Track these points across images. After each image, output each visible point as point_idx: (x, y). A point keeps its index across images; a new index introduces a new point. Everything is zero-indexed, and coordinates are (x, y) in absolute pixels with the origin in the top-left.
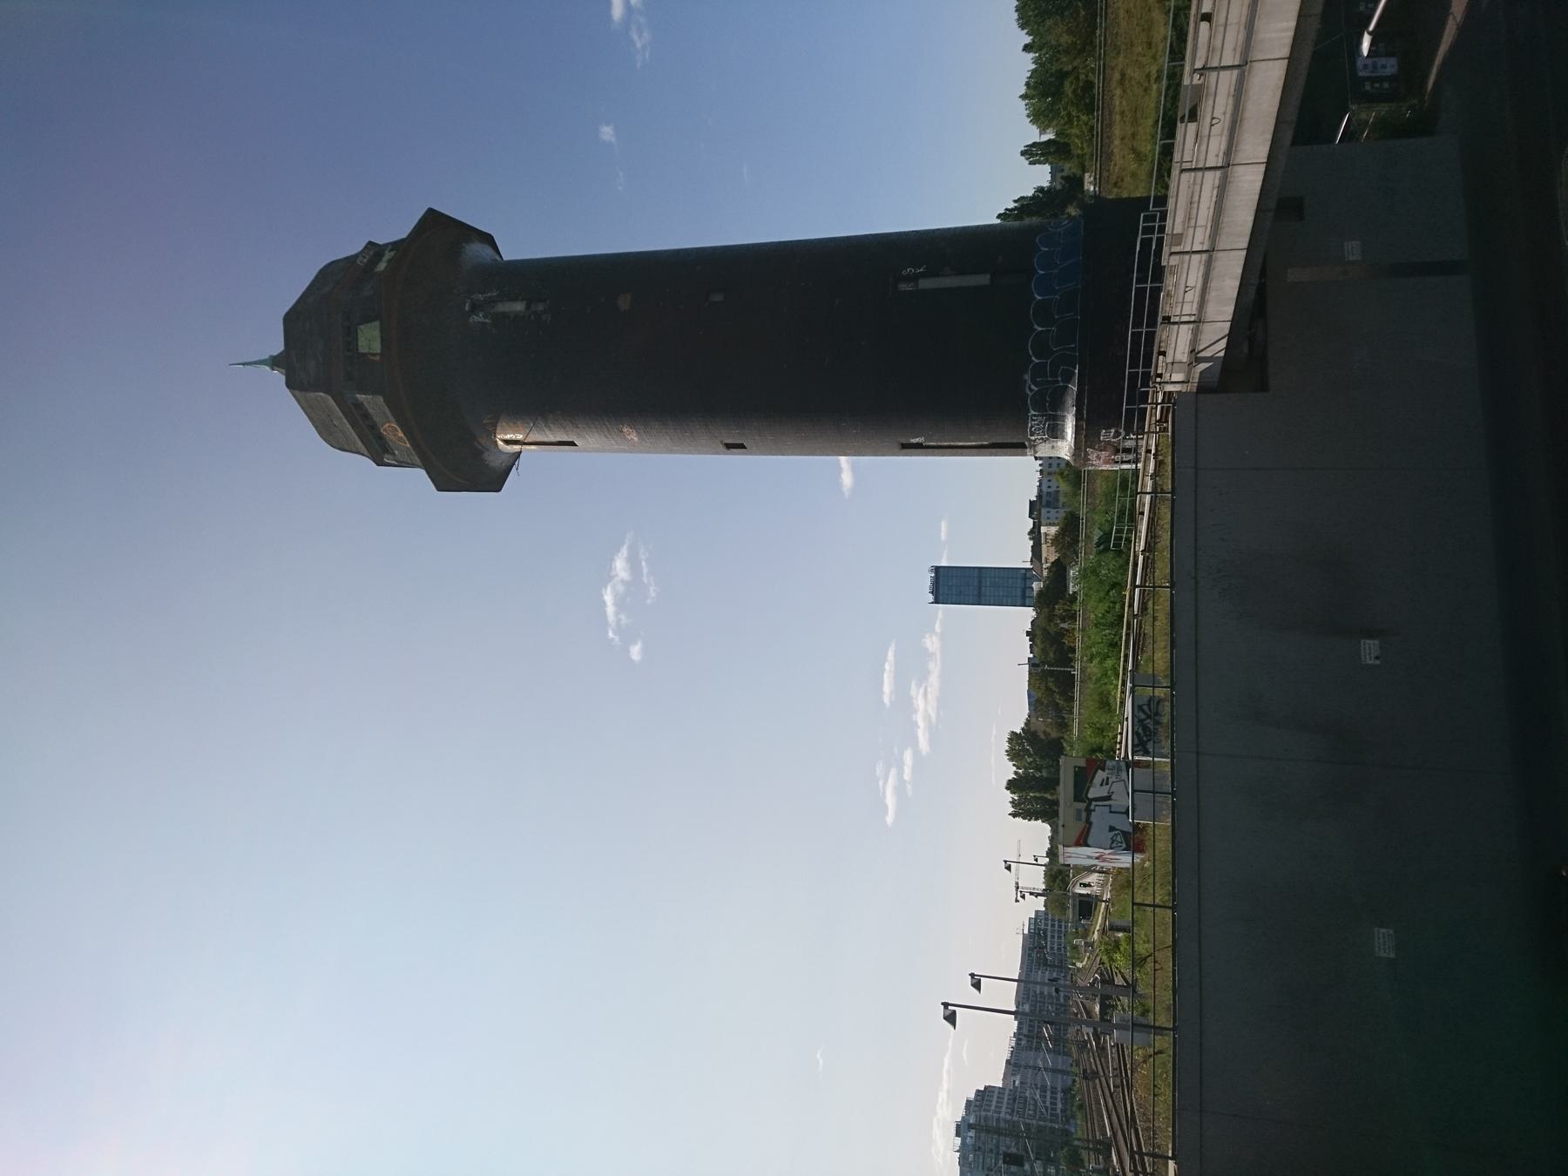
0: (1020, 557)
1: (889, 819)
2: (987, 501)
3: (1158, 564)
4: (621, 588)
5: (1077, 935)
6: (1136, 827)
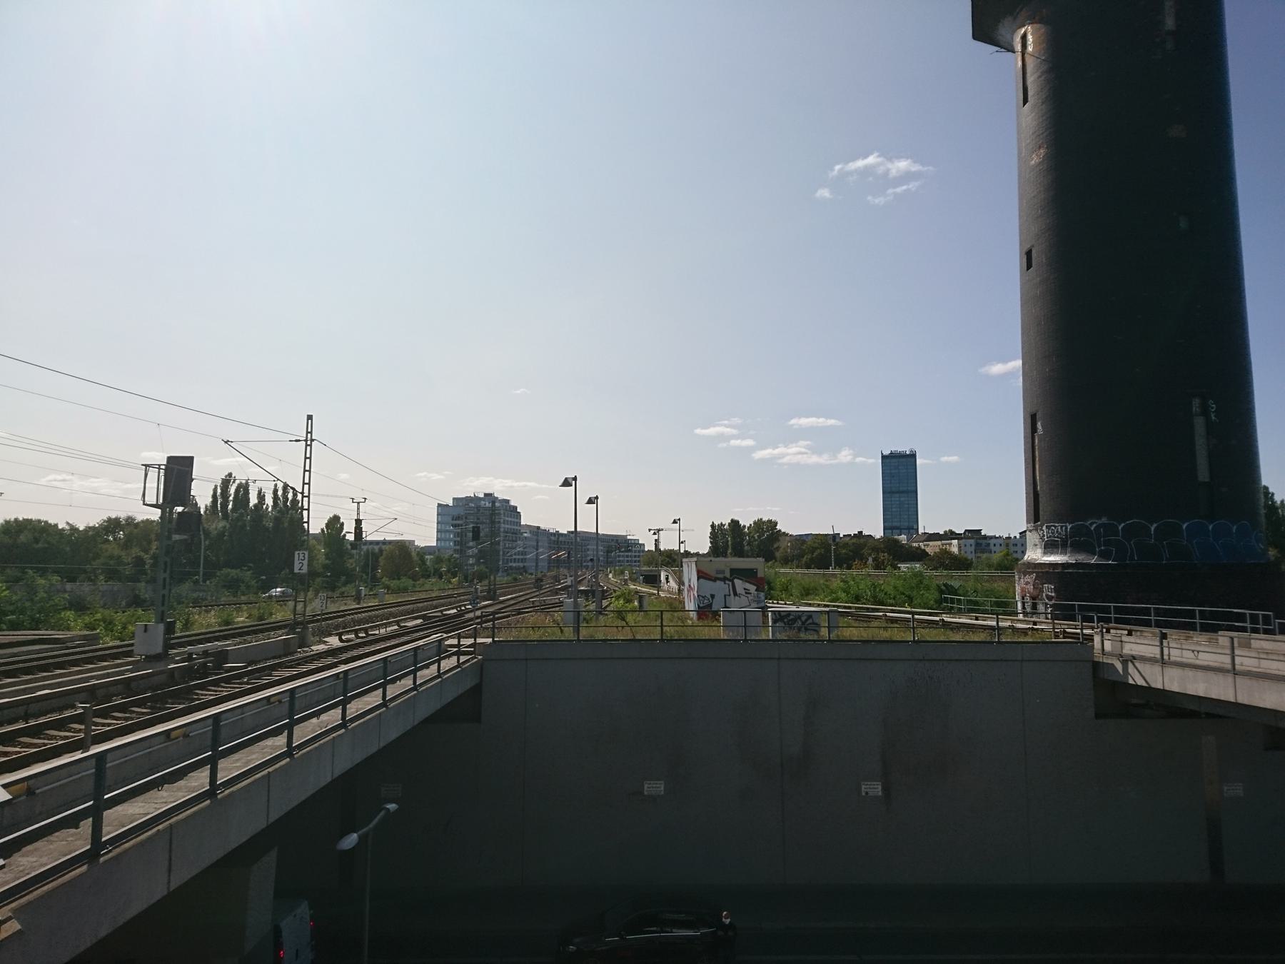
0: (929, 521)
1: (698, 431)
2: (983, 489)
3: (935, 632)
4: (881, 170)
5: (631, 573)
6: (716, 614)
